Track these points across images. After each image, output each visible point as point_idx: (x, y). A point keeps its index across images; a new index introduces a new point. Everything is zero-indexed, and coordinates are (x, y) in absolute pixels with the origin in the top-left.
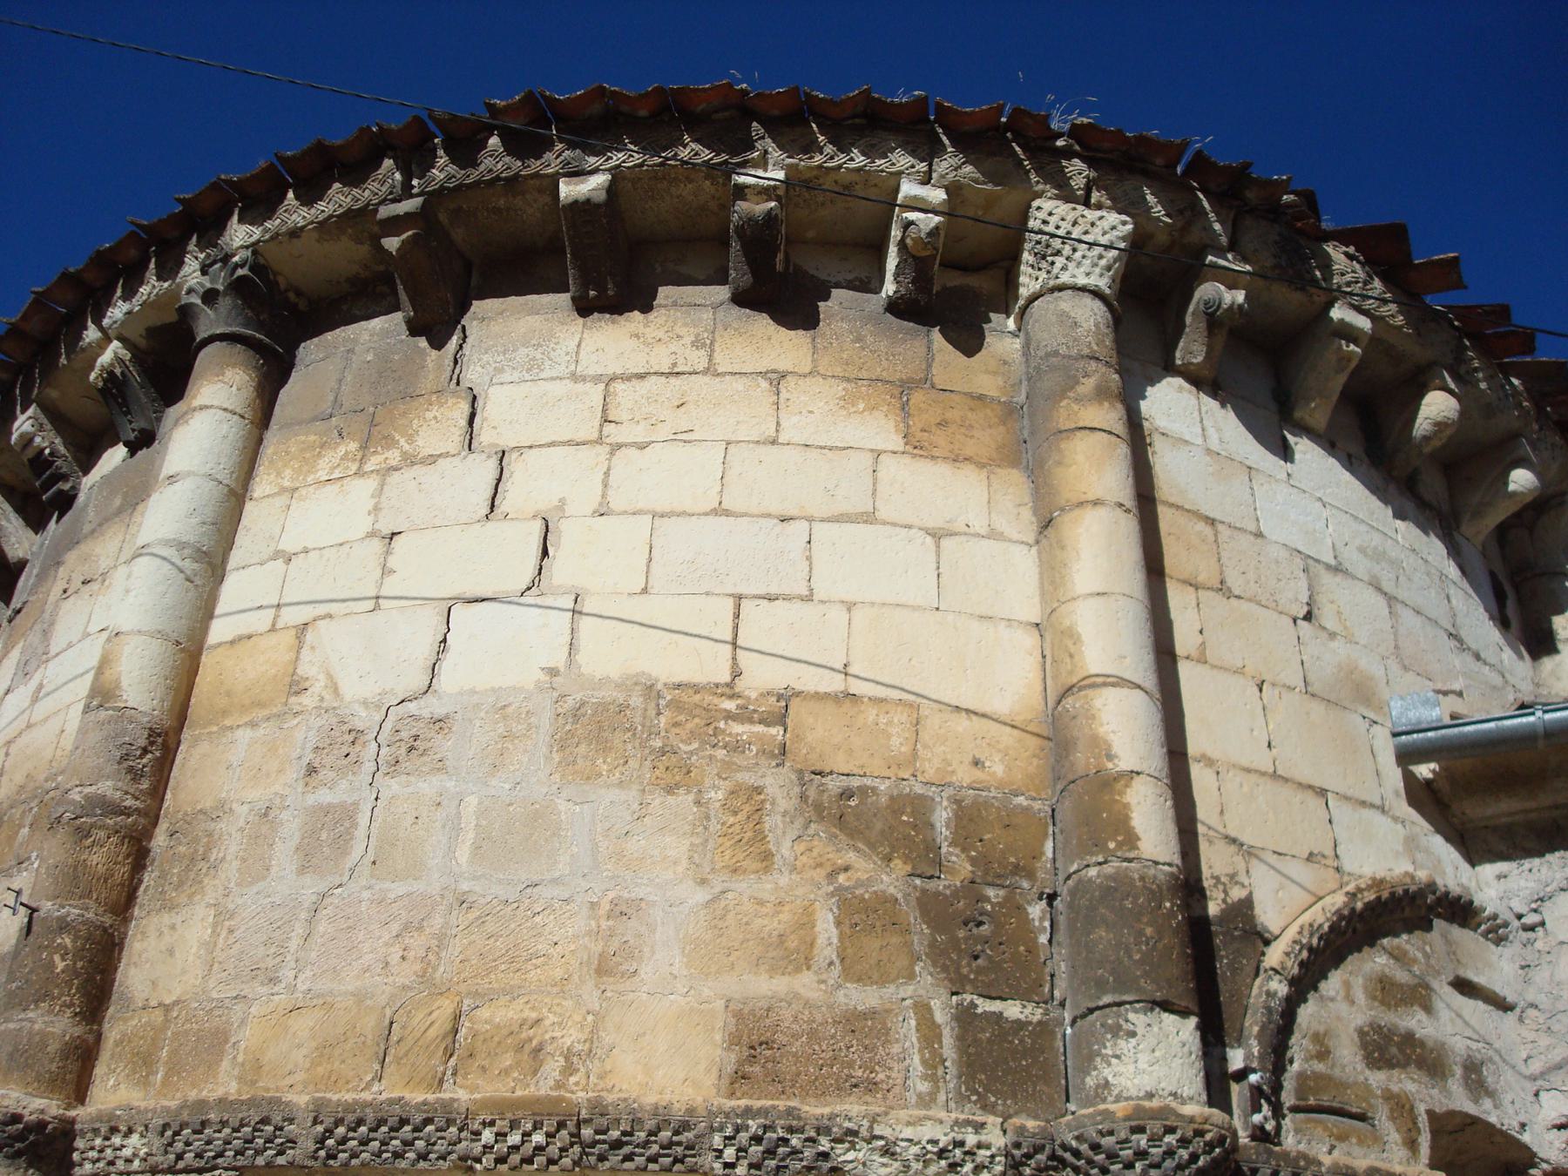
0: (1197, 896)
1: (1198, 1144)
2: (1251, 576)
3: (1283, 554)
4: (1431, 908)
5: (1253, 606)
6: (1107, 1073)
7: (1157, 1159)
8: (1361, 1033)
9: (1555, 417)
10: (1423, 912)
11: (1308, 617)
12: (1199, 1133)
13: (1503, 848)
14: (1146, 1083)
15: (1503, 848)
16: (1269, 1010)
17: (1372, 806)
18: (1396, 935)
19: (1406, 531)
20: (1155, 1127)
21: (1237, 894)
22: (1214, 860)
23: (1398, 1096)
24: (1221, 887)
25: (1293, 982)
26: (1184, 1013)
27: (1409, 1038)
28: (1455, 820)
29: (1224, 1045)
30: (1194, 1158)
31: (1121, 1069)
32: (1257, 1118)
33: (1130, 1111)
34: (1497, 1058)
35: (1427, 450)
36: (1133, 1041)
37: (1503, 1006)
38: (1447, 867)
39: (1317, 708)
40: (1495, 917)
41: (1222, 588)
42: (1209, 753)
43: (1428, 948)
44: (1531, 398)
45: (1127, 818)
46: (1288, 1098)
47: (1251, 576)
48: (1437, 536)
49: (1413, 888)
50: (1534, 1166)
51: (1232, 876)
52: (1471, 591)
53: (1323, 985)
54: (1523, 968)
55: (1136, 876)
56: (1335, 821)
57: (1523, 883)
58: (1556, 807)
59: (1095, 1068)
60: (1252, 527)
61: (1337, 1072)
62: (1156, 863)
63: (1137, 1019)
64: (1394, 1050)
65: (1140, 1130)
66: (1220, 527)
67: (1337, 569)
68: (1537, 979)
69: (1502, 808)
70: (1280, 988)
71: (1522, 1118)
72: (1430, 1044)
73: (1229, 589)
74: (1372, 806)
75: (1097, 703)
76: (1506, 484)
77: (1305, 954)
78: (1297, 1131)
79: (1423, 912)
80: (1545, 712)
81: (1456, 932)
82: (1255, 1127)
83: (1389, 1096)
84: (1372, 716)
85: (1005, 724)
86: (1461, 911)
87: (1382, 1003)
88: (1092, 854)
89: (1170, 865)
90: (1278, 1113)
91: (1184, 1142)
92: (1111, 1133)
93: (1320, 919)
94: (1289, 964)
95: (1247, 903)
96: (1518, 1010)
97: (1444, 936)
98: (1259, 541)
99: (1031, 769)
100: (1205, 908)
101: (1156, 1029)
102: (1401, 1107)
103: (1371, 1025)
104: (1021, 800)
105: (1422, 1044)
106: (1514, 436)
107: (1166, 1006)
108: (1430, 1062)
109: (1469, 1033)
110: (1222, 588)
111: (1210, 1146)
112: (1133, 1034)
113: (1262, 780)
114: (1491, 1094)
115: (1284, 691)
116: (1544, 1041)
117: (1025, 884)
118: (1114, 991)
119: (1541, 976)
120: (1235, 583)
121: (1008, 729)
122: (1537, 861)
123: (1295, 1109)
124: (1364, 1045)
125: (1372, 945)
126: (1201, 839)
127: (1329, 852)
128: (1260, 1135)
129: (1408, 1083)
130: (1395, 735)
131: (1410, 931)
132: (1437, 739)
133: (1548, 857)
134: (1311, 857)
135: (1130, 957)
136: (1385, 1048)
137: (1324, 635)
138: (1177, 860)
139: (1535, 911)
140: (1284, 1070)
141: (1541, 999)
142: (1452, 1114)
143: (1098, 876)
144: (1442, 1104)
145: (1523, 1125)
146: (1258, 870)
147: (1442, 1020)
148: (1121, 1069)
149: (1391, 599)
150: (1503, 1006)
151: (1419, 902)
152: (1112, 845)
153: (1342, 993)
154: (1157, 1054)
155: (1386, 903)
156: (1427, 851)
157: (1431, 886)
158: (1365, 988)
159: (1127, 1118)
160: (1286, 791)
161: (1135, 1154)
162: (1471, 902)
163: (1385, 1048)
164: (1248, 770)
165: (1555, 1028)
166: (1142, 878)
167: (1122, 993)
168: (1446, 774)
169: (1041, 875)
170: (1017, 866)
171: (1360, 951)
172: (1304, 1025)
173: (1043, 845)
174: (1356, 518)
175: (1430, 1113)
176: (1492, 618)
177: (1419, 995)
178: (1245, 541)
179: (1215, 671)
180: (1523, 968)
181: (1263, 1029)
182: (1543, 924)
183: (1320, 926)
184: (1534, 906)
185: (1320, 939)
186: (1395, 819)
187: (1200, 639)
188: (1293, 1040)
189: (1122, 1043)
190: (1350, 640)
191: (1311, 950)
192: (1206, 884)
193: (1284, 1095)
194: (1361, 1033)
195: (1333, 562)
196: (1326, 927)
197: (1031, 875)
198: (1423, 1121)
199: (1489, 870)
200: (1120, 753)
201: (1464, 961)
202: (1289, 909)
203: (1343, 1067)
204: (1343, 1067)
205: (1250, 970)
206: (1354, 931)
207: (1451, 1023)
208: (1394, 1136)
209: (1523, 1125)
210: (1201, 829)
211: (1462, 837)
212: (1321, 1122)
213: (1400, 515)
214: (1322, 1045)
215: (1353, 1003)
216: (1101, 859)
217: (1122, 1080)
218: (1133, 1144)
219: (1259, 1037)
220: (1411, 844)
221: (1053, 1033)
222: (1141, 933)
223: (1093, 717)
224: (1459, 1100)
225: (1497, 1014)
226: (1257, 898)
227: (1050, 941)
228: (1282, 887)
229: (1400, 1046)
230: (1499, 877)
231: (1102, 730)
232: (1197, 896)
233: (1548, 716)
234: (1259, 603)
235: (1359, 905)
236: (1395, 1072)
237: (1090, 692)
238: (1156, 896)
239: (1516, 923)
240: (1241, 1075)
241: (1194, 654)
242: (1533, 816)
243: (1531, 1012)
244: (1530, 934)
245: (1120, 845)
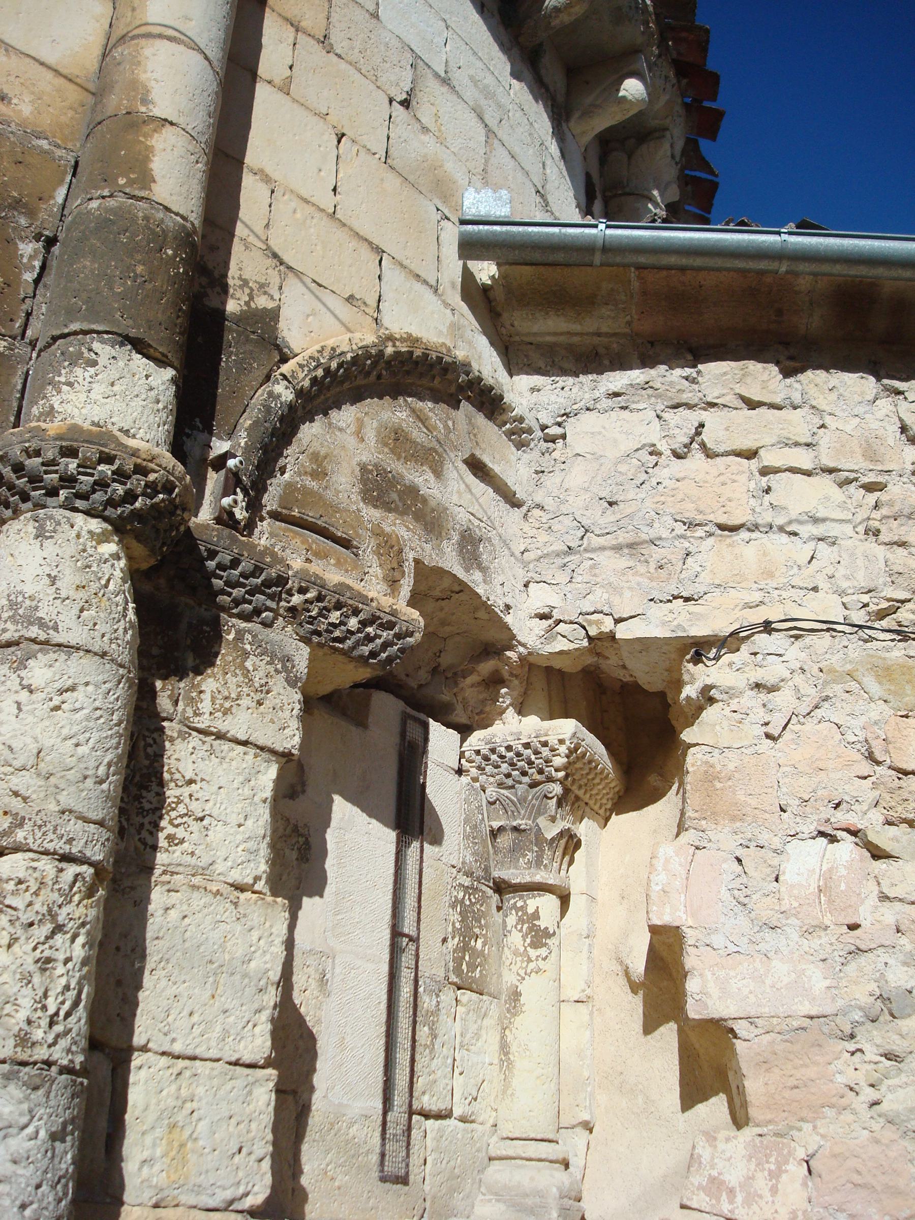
0: (218, 289)
1: (137, 483)
2: (357, 44)
3: (394, 42)
4: (461, 388)
5: (352, 71)
6: (55, 401)
7: (85, 488)
8: (363, 468)
9: (675, 56)
10: (453, 389)
11: (406, 103)
12: (141, 470)
13: (541, 364)
14: (97, 413)
15: (541, 364)
16: (268, 409)
17: (425, 282)
18: (421, 399)
19: (519, 91)
20: (89, 451)
21: (262, 302)
22: (244, 264)
23: (389, 536)
24: (247, 291)
25: (300, 393)
26: (162, 362)
27: (412, 491)
28: (504, 331)
29: (211, 433)
30: (130, 497)
31: (72, 396)
32: (226, 501)
33: (64, 430)
34: (496, 541)
35: (555, 22)
36: (92, 370)
37: (514, 502)
38: (487, 362)
39: (392, 182)
40: (521, 420)
41: (324, 41)
42: (269, 170)
43: (450, 423)
44: (658, 22)
45: (147, 160)
46: (270, 500)
47: (357, 44)
48: (545, 106)
49: (447, 359)
50: (511, 648)
51: (262, 286)
52: (565, 173)
53: (334, 414)
54: (537, 472)
55: (141, 214)
56: (385, 279)
57: (553, 398)
58: (599, 335)
59: (45, 397)
60: (372, 8)
61: (329, 494)
62: (167, 209)
63: (103, 350)
64: (394, 496)
65: (71, 452)
66: (385, 256)
67: (445, 81)
68: (548, 483)
69: (549, 326)
70: (287, 395)
71: (509, 601)
72: (433, 503)
73: (331, 45)
74: (425, 282)
75: (147, 52)
76: (618, 90)
77: (320, 372)
78: (272, 535)
79: (453, 389)
80: (608, 227)
81: (480, 419)
82: (223, 509)
83: (378, 532)
84: (446, 212)
85: (49, 67)
86: (490, 403)
87: (392, 451)
88: (96, 188)
89: (182, 217)
90: (254, 506)
91: (121, 475)
92: (37, 453)
93: (345, 348)
94: (301, 375)
95: (273, 316)
96: (524, 509)
97: (469, 419)
98: (374, 21)
99: (63, 119)
100: (224, 303)
101: (121, 364)
102: (390, 549)
103: (375, 465)
104: (44, 144)
105: (425, 501)
106: (634, 51)
107: (139, 346)
108: (431, 521)
109: (475, 509)
110: (324, 41)
111: (152, 489)
112: (94, 364)
113: (318, 215)
114: (483, 570)
115: (362, 152)
116: (543, 537)
117: (23, 221)
118: (85, 319)
119: (551, 482)
120: (338, 39)
121: (50, 75)
122: (570, 380)
123: (275, 516)
124: (364, 481)
125: (394, 398)
126: (236, 240)
127: (373, 303)
128: (225, 519)
129: (401, 529)
130: (463, 222)
131: (436, 401)
132: (501, 233)
133: (582, 378)
134: (350, 299)
135: (111, 289)
136: (379, 488)
137: (417, 126)
138: (195, 218)
139: (559, 424)
140: (272, 475)
141: (549, 503)
142: (440, 572)
143: (99, 208)
144: (432, 558)
145: (508, 607)
146: (293, 288)
147: (449, 489)
148: (72, 396)
149: (490, 132)
150: (514, 502)
151: (449, 376)
152: (122, 181)
153: (353, 428)
154: (116, 388)
155: (417, 363)
156: (470, 343)
157: (466, 367)
158: (379, 433)
159: (59, 437)
160: (341, 235)
161: (61, 479)
162: (501, 398)
163: (379, 488)
164: (307, 201)
165: (554, 528)
166: (146, 218)
167: (90, 322)
168: (503, 280)
169: (42, 215)
170: (18, 201)
171: (381, 398)
172: (305, 442)
173: (54, 190)
174: (475, 53)
175: (417, 562)
176: (578, 206)
177: (432, 460)
178: (360, 16)
179: (295, 105)
180: (537, 472)
181: (256, 423)
182: (564, 437)
183: (343, 353)
184: (559, 419)
185: (340, 365)
186: (446, 305)
187: (288, 73)
188: (289, 451)
189: (78, 371)
190: (441, 141)
191: (327, 371)
192: (230, 282)
193: (266, 499)
194: (363, 468)
195: (443, 74)
196: (349, 356)
197: (31, 213)
198: (409, 567)
199: (524, 381)
200: (156, 99)
201: (483, 446)
202: (313, 331)
203: (338, 492)
204: (338, 492)
205: (261, 373)
206: (379, 377)
207: (458, 494)
208: (376, 570)
209: (508, 607)
210: (240, 230)
211: (507, 348)
212: (301, 535)
213: (515, 75)
214: (319, 466)
215: (362, 440)
216: (106, 193)
217: (69, 408)
218: (61, 467)
219: (249, 430)
220: (455, 328)
221: (13, 368)
222: (130, 268)
223: (139, 63)
224: (449, 560)
225: (504, 506)
226: (283, 313)
227: (37, 281)
228: (313, 313)
229: (401, 494)
230: (533, 390)
231: (143, 77)
232: (218, 289)
233: (609, 232)
234: (360, 71)
235: (390, 350)
236: (391, 516)
237: (143, 42)
238: (159, 239)
239: (539, 434)
240: (220, 463)
241: (277, 81)
242: (576, 340)
243: (536, 512)
244: (550, 445)
245: (131, 183)
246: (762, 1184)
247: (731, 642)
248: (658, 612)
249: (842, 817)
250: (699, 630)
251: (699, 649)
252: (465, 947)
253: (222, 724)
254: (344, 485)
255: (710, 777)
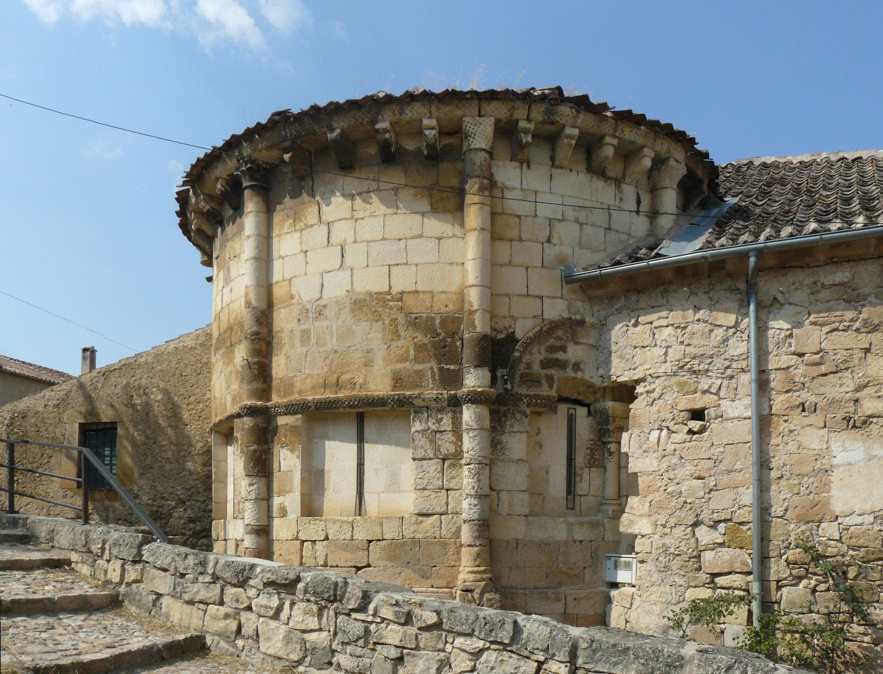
8: (541, 361)
21: (510, 330)
27: (557, 360)
114: (581, 370)
246: (641, 508)
247: (643, 380)
248: (626, 373)
249: (664, 424)
250: (636, 378)
251: (638, 382)
252: (592, 458)
253: (512, 430)
254: (536, 367)
255: (634, 417)
